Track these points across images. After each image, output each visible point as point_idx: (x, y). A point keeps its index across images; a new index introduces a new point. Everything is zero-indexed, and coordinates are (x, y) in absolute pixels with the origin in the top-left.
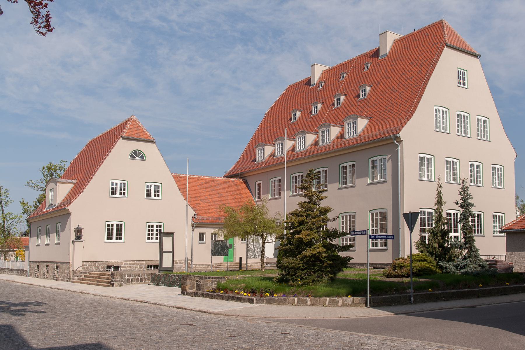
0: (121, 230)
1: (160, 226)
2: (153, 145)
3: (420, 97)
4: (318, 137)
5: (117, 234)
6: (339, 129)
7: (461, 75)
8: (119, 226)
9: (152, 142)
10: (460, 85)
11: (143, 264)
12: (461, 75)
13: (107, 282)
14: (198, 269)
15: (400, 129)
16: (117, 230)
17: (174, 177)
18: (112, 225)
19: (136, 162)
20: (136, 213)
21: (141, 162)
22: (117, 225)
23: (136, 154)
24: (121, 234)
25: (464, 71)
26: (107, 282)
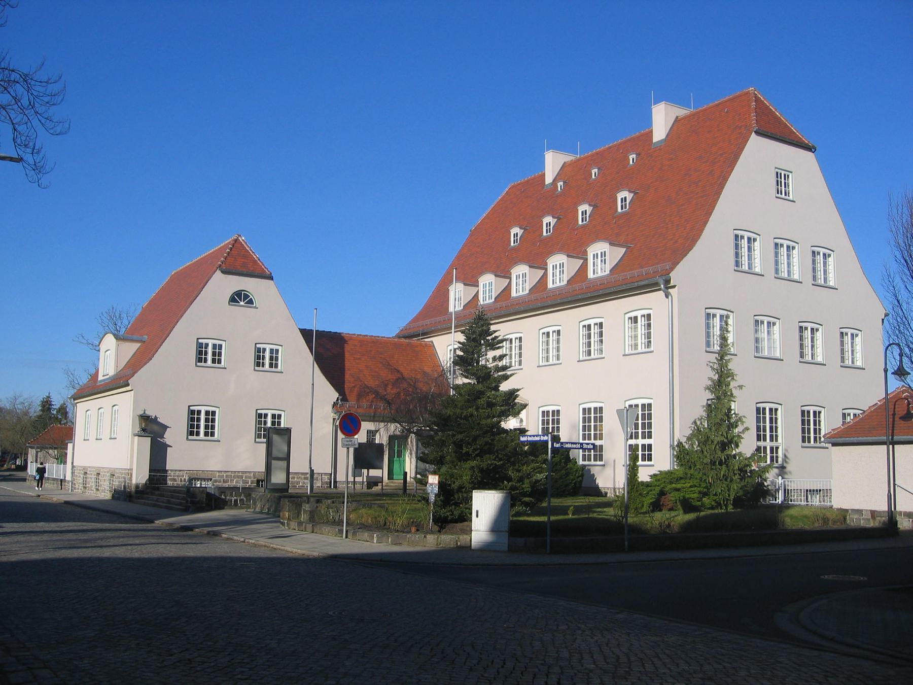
0: (213, 421)
1: (279, 416)
2: (810, 155)
3: (709, 214)
4: (510, 283)
5: (206, 427)
6: (541, 272)
7: (781, 180)
8: (211, 415)
9: (271, 278)
10: (779, 195)
11: (250, 477)
12: (781, 180)
13: (180, 504)
14: (800, 525)
15: (672, 269)
16: (207, 420)
17: (307, 334)
18: (199, 412)
19: (241, 310)
20: (238, 395)
21: (249, 311)
22: (207, 413)
23: (238, 297)
24: (213, 427)
25: (787, 173)
26: (180, 504)
